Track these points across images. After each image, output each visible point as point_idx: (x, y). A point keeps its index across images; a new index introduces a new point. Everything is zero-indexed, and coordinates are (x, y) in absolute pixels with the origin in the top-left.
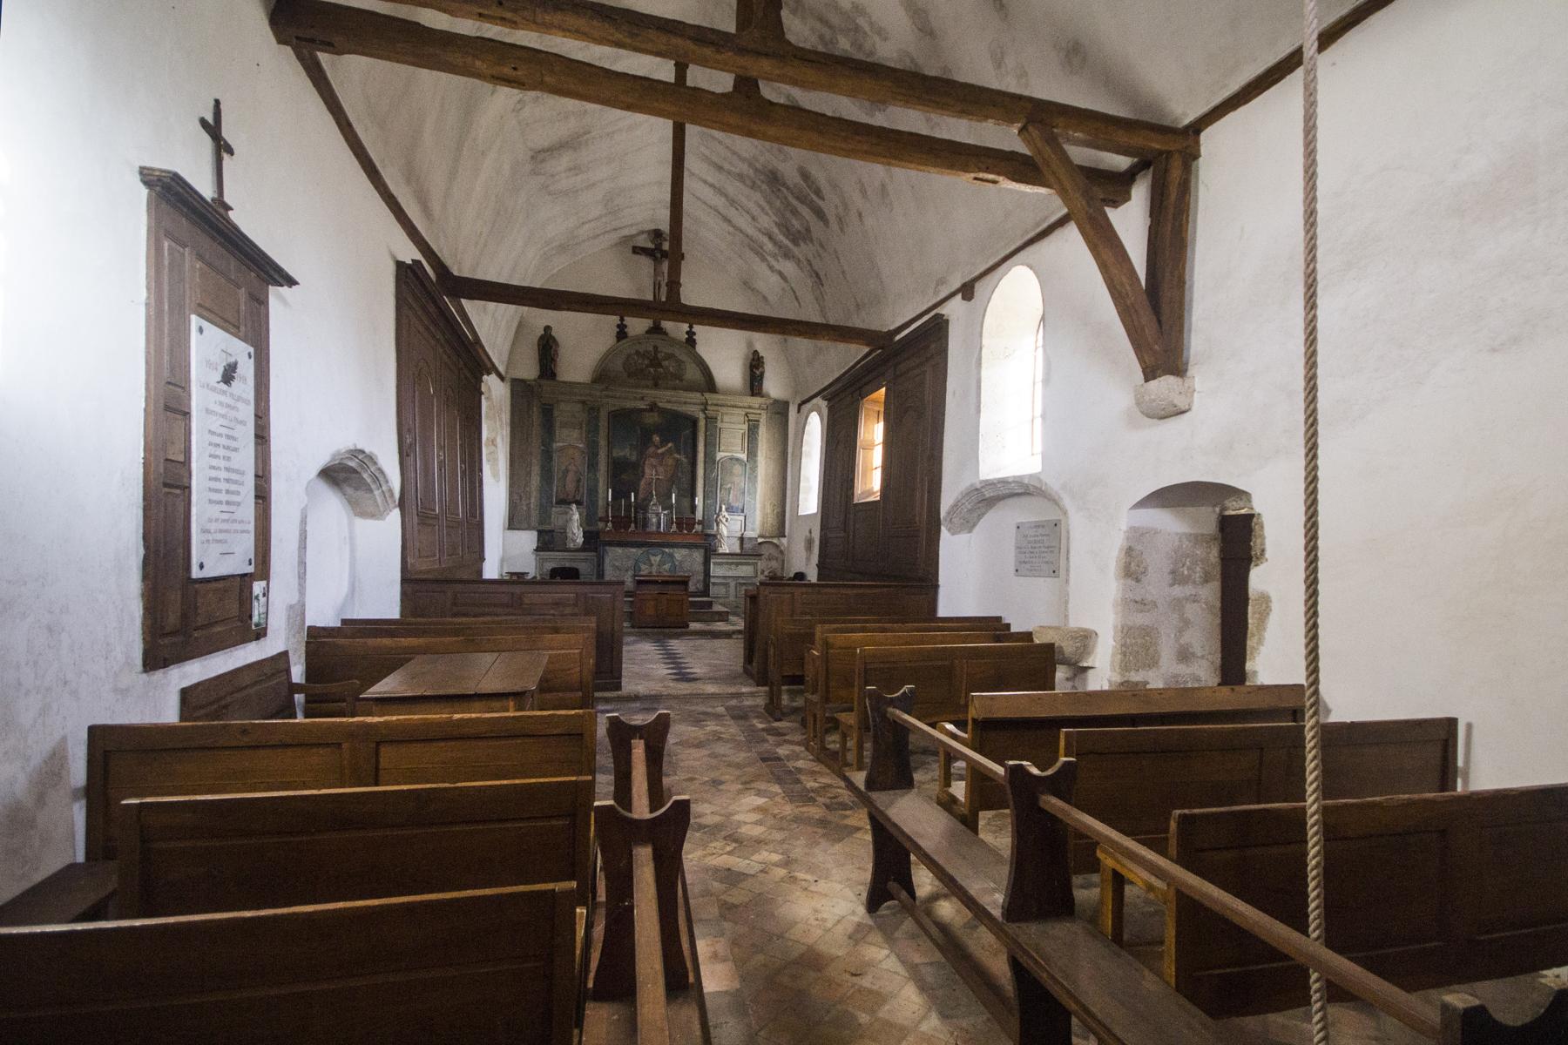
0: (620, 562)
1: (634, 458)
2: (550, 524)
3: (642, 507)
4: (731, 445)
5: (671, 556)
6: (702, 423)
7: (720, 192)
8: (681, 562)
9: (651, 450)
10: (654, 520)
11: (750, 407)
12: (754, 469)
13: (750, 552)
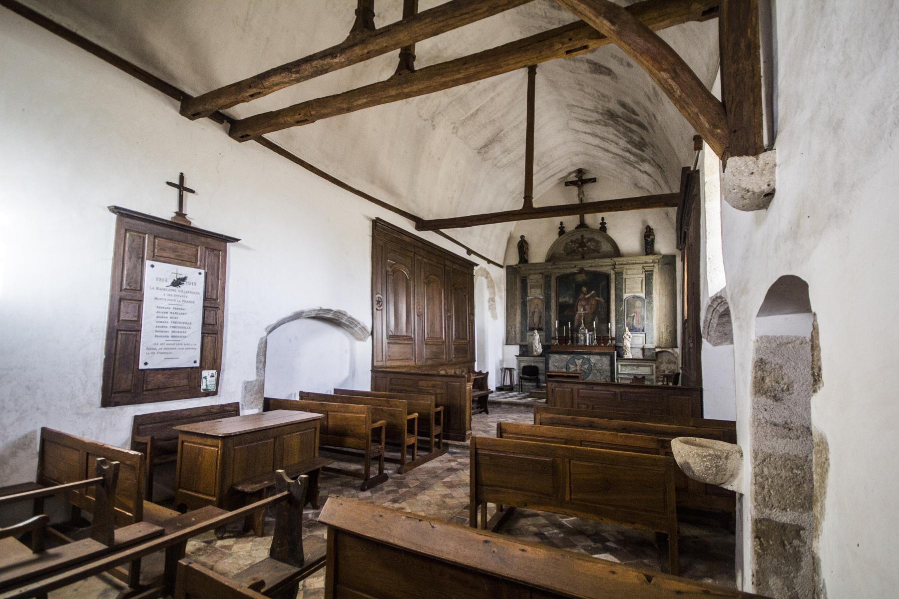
0: (557, 363)
1: (571, 302)
2: (526, 341)
3: (575, 330)
4: (634, 287)
5: (589, 360)
6: (613, 277)
7: (595, 135)
8: (595, 364)
9: (582, 296)
10: (582, 338)
11: (646, 263)
12: (650, 302)
13: (650, 358)
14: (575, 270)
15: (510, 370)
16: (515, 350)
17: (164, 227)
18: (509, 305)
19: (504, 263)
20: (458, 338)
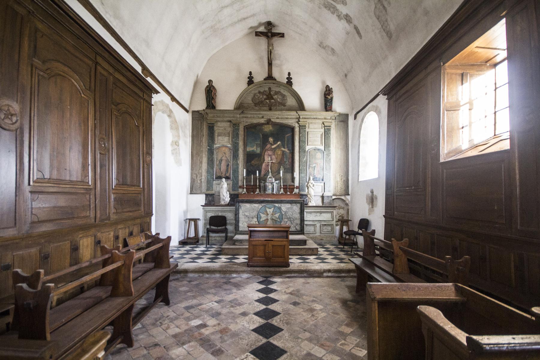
1: (258, 151)
3: (263, 179)
5: (280, 208)
6: (297, 130)
8: (286, 212)
9: (269, 146)
11: (325, 119)
12: (329, 155)
14: (262, 121)
15: (195, 220)
16: (201, 199)
17: (381, 267)
18: (195, 152)
19: (189, 108)
20: (122, 182)
